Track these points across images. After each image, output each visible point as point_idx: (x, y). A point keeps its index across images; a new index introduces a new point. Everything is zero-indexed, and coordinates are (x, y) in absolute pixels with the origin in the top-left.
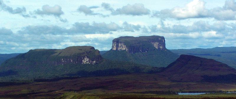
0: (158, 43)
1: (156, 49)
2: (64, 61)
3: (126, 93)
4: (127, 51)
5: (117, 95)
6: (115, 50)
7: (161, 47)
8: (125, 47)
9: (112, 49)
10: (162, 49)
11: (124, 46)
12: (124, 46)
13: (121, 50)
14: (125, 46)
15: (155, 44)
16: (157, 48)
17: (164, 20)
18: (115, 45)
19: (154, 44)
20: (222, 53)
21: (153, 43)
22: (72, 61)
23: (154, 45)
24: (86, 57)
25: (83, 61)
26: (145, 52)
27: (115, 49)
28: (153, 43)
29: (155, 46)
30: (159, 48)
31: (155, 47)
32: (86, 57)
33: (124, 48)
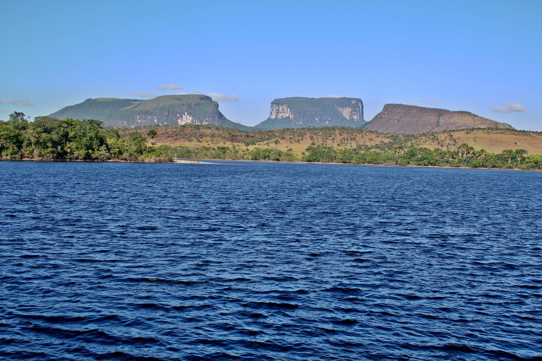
0: (350, 110)
1: (347, 119)
2: (141, 121)
3: (487, 341)
4: (291, 118)
5: (216, 225)
6: (274, 118)
7: (355, 117)
8: (288, 112)
9: (269, 119)
10: (357, 119)
11: (287, 110)
12: (287, 110)
13: (282, 118)
14: (289, 110)
15: (345, 112)
16: (348, 118)
17: (445, 151)
19: (343, 111)
21: (342, 110)
22: (156, 121)
23: (342, 113)
24: (186, 113)
25: (179, 121)
27: (273, 117)
28: (342, 110)
29: (344, 115)
30: (352, 119)
31: (344, 117)
32: (186, 113)
33: (287, 113)
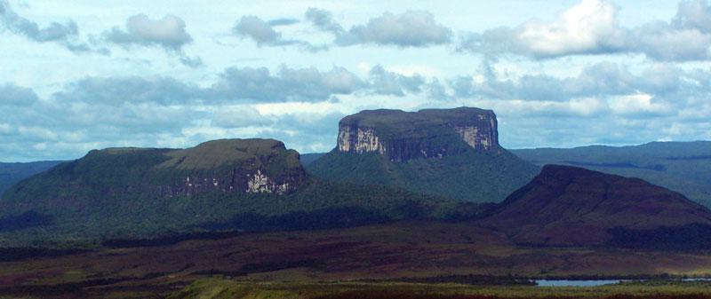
0: (476, 131)
1: (471, 147)
2: (193, 186)
3: (380, 281)
4: (382, 153)
5: (352, 286)
6: (348, 150)
7: (485, 143)
8: (377, 142)
9: (336, 149)
10: (488, 147)
11: (374, 140)
12: (374, 140)
13: (364, 150)
14: (377, 139)
15: (467, 134)
16: (473, 144)
17: (495, 61)
18: (347, 135)
19: (463, 133)
21: (461, 131)
22: (216, 184)
23: (463, 137)
24: (259, 172)
25: (250, 183)
27: (346, 148)
28: (461, 131)
29: (466, 140)
30: (479, 146)
32: (259, 172)
33: (374, 144)
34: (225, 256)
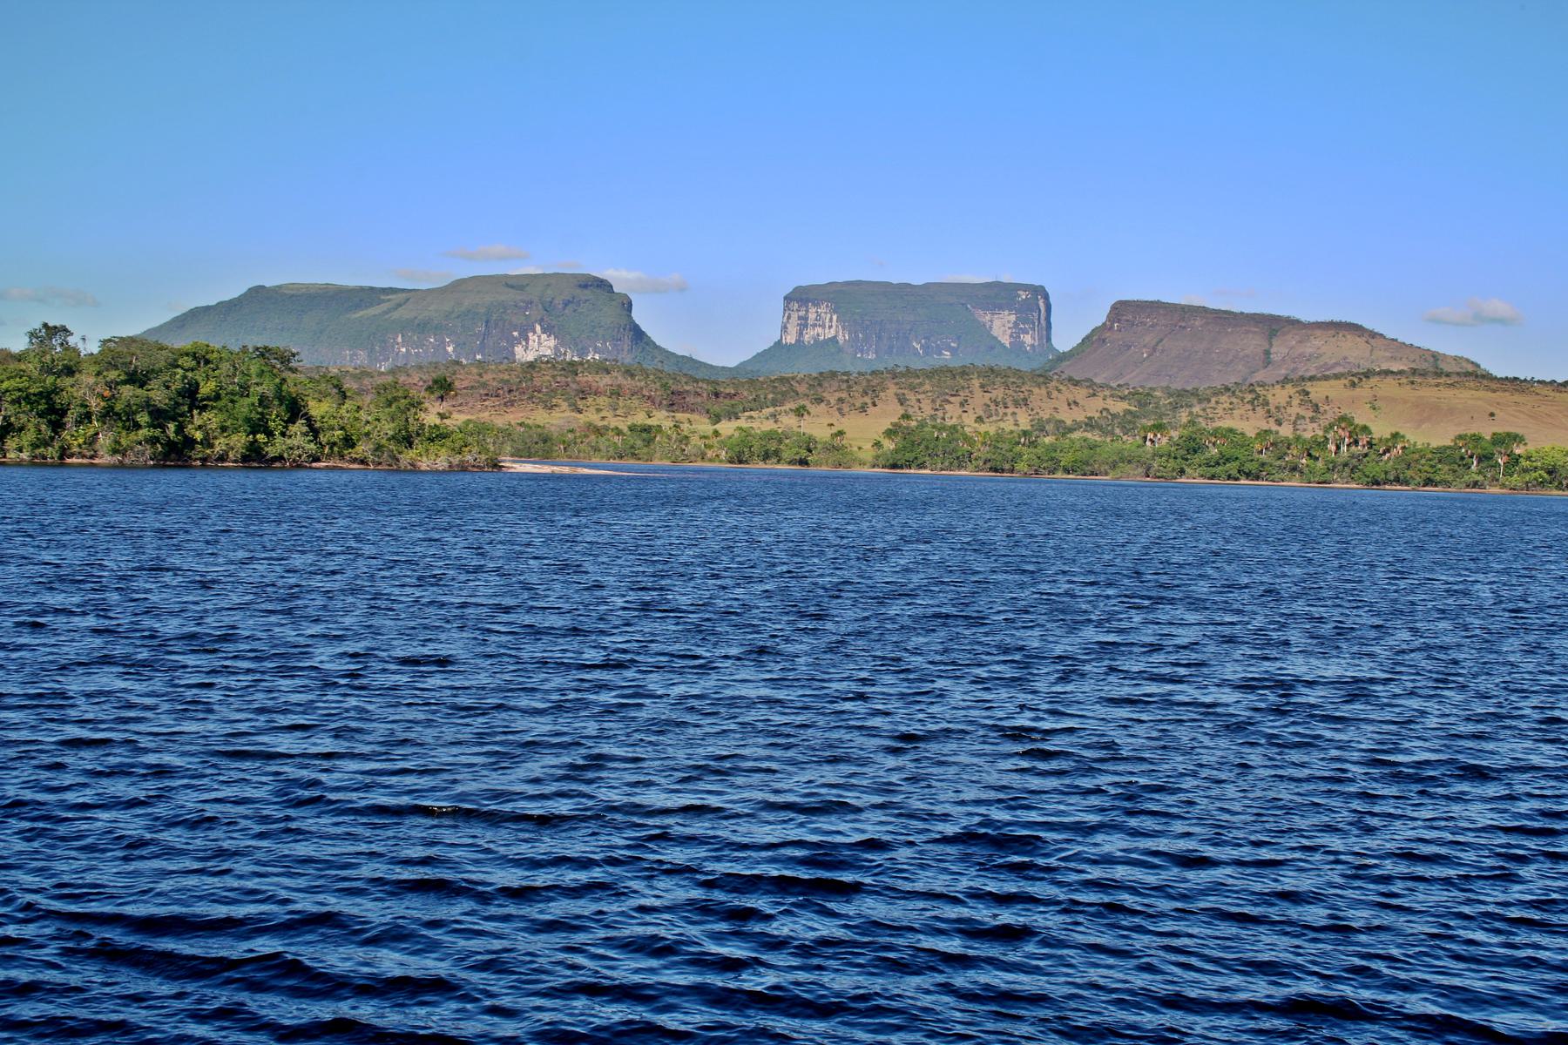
0: (1013, 318)
1: (1003, 346)
2: (408, 350)
3: (1408, 987)
4: (841, 342)
5: (625, 651)
6: (793, 342)
7: (1028, 339)
8: (834, 324)
9: (779, 343)
10: (1032, 346)
11: (831, 320)
12: (831, 320)
13: (816, 340)
14: (835, 317)
15: (997, 323)
16: (1006, 340)
18: (795, 316)
19: (991, 321)
20: (1338, 830)
21: (988, 318)
22: (450, 349)
23: (991, 327)
24: (538, 328)
25: (519, 350)
26: (941, 354)
27: (791, 339)
28: (988, 318)
29: (995, 333)
30: (1018, 346)
32: (538, 328)
33: (830, 327)
34: (620, 665)
